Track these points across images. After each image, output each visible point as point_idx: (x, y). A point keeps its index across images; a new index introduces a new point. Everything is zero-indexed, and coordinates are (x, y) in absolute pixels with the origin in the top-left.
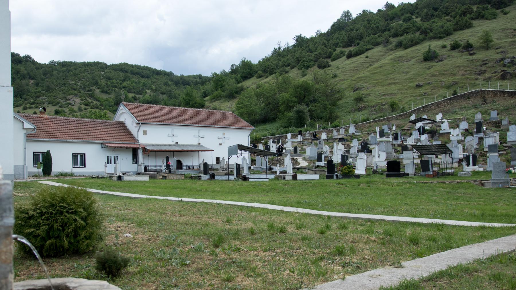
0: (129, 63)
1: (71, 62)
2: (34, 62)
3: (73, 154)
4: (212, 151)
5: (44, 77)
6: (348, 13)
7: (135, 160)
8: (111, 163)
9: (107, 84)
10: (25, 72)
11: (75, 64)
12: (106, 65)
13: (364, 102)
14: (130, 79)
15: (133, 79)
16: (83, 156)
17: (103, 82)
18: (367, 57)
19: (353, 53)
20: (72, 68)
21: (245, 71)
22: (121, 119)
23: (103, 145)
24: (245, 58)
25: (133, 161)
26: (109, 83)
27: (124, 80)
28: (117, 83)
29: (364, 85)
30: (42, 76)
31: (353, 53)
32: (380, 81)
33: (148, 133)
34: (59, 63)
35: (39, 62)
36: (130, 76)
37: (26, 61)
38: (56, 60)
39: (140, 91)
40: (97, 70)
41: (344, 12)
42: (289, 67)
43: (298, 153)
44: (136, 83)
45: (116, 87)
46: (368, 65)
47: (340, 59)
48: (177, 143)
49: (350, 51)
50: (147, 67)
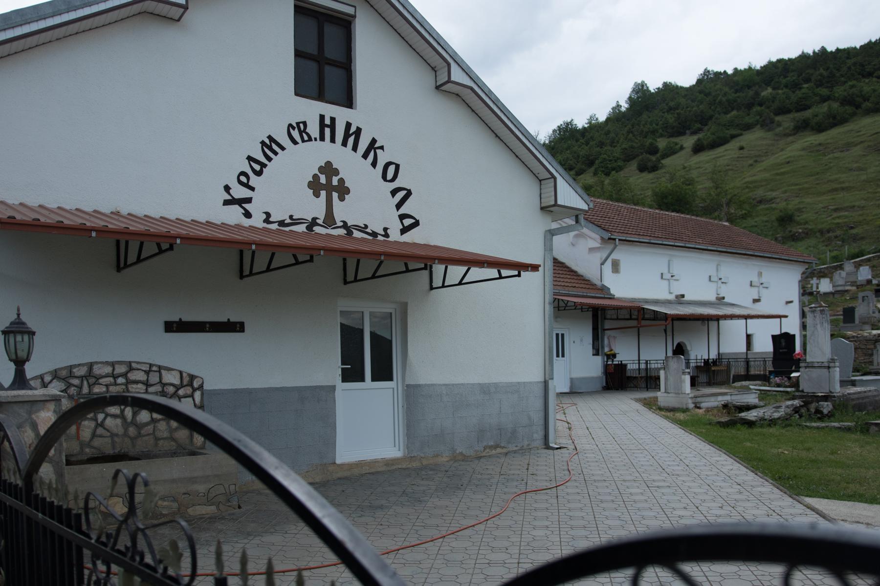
4: (780, 317)
6: (643, 86)
13: (799, 224)
18: (742, 148)
19: (705, 143)
29: (774, 194)
31: (705, 143)
32: (806, 186)
41: (636, 85)
46: (751, 162)
48: (683, 296)
49: (699, 140)
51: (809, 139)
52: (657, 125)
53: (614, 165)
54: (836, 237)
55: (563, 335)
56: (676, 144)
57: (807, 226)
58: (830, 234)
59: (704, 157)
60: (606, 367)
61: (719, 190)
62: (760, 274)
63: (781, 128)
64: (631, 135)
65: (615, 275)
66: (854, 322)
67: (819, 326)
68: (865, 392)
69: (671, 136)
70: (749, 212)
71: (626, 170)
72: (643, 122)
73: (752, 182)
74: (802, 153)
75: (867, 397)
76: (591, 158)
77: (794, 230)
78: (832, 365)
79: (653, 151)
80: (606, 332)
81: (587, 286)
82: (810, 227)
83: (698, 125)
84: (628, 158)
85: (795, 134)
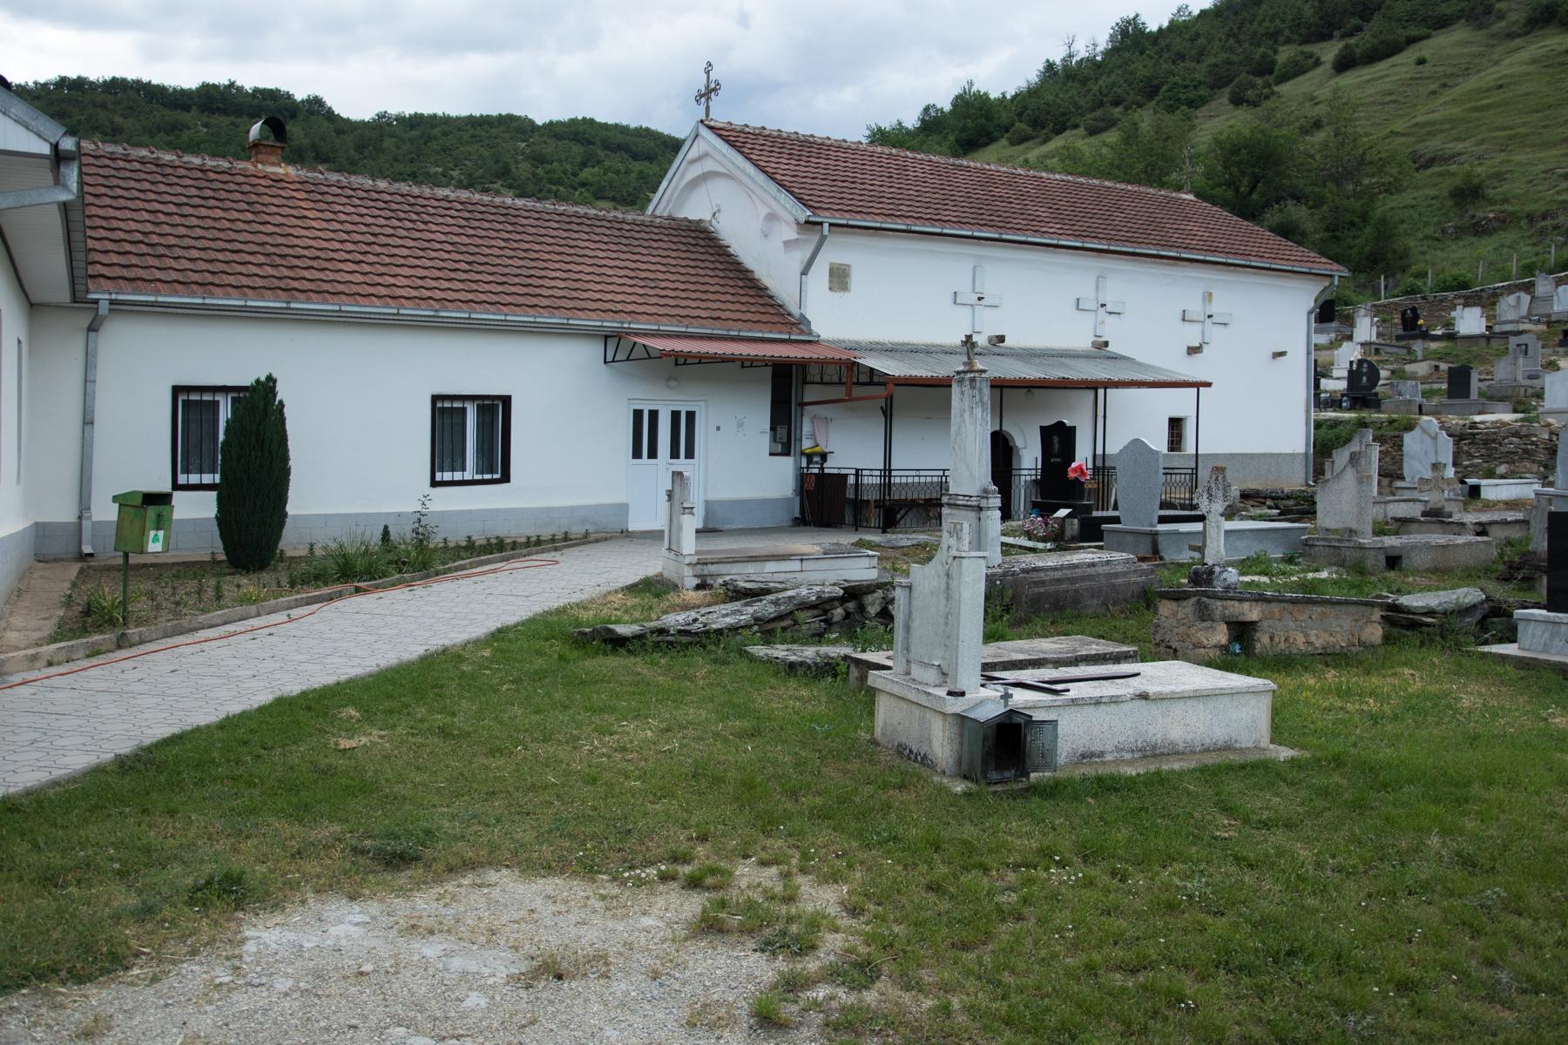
0: (598, 120)
1: (435, 116)
2: (330, 116)
3: (435, 399)
4: (1197, 385)
5: (357, 156)
7: (782, 432)
8: (653, 454)
9: (534, 175)
10: (306, 142)
11: (446, 121)
12: (532, 122)
13: (1492, 202)
14: (599, 162)
15: (607, 163)
16: (496, 410)
17: (523, 169)
18: (1421, 62)
20: (436, 131)
21: (970, 124)
22: (695, 209)
23: (621, 349)
24: (971, 84)
25: (774, 439)
26: (540, 171)
27: (584, 165)
28: (565, 172)
29: (1459, 146)
30: (352, 152)
31: (1358, 51)
32: (1523, 130)
33: (855, 279)
34: (400, 119)
35: (344, 115)
36: (601, 153)
37: (311, 113)
38: (393, 110)
39: (630, 194)
40: (507, 136)
42: (1119, 109)
43: (1474, 395)
44: (617, 172)
45: (559, 182)
46: (1433, 87)
47: (1308, 75)
48: (1001, 339)
50: (647, 129)
51: (1548, 42)
52: (1283, 21)
53: (1192, 94)
54: (1556, 227)
55: (691, 416)
56: (1311, 56)
57: (1506, 207)
58: (1548, 223)
59: (1349, 79)
60: (802, 478)
61: (1340, 138)
62: (1208, 297)
63: (1503, 24)
64: (1232, 40)
65: (837, 295)
66: (1467, 396)
67: (967, 415)
68: (1093, 565)
69: (1307, 40)
70: (1396, 179)
71: (1213, 104)
72: (1259, 18)
73: (1425, 124)
74: (1532, 68)
75: (1090, 577)
76: (1155, 82)
77: (1480, 214)
78: (983, 503)
79: (1265, 68)
80: (807, 408)
81: (776, 319)
82: (1510, 209)
83: (1355, 21)
84: (1219, 81)
85: (1526, 34)
